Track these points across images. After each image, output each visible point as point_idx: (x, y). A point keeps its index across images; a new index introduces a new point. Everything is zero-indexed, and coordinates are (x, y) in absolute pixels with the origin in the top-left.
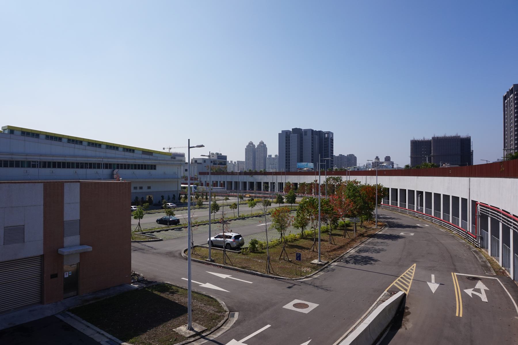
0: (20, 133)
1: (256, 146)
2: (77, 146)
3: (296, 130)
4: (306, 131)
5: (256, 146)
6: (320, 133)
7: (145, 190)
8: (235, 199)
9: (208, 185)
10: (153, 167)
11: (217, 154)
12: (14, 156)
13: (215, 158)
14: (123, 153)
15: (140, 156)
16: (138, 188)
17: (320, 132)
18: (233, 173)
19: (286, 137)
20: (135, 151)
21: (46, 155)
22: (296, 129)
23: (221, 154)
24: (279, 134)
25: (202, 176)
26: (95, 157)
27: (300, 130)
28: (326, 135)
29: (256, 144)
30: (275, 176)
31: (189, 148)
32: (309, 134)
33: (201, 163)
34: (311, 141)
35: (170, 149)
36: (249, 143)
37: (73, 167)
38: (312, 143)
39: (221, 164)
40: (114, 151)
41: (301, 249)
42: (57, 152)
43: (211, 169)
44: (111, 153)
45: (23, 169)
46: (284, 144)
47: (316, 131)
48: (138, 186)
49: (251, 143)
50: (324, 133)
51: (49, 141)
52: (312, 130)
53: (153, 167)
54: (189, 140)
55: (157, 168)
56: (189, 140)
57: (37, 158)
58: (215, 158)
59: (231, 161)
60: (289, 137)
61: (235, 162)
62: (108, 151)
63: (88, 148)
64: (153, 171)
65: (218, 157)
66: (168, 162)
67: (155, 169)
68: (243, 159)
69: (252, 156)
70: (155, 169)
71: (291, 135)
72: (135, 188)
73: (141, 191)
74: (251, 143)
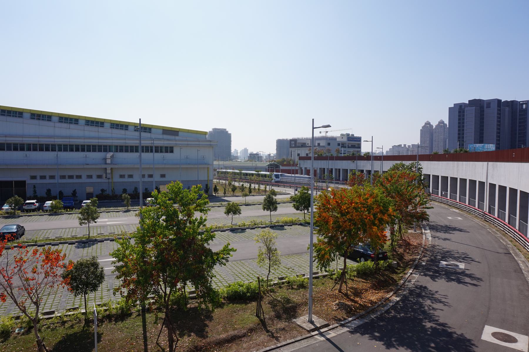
0: (29, 115)
1: (434, 127)
2: (72, 126)
3: (473, 103)
4: (489, 103)
5: (434, 127)
6: (513, 104)
7: (84, 180)
8: (279, 198)
9: (308, 172)
10: (170, 150)
11: (348, 135)
12: (24, 139)
13: (345, 139)
14: (110, 130)
15: (161, 137)
16: (126, 176)
17: (512, 102)
18: (368, 157)
19: (459, 112)
20: (153, 130)
21: (30, 136)
22: (475, 100)
23: (353, 135)
24: (450, 108)
25: (302, 162)
26: (85, 138)
27: (480, 101)
28: (524, 106)
29: (434, 124)
30: (378, 163)
31: (313, 128)
32: (495, 106)
33: (324, 147)
34: (496, 115)
35: (327, 132)
36: (439, 123)
37: (161, 152)
38: (499, 118)
39: (353, 146)
40: (123, 132)
41: (238, 342)
42: (91, 136)
43: (315, 153)
44: (92, 132)
45: (162, 154)
46: (457, 121)
47: (506, 102)
48: (127, 173)
49: (428, 124)
50: (521, 104)
51: (36, 122)
52: (499, 101)
53: (170, 150)
54: (313, 120)
55: (175, 150)
56: (313, 120)
57: (18, 140)
58: (345, 139)
59: (405, 145)
60: (464, 112)
61: (409, 146)
62: (115, 131)
63: (87, 128)
64: (168, 155)
65: (348, 138)
66: (189, 143)
67: (172, 151)
68: (417, 141)
69: (428, 139)
70: (172, 151)
71: (466, 109)
72: (122, 176)
73: (130, 180)
74: (428, 124)
